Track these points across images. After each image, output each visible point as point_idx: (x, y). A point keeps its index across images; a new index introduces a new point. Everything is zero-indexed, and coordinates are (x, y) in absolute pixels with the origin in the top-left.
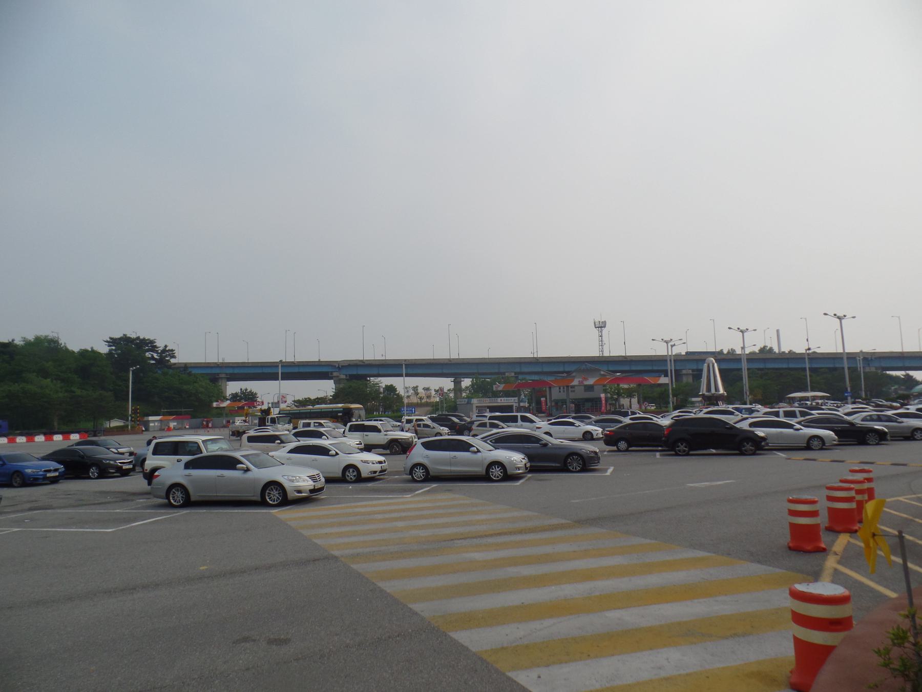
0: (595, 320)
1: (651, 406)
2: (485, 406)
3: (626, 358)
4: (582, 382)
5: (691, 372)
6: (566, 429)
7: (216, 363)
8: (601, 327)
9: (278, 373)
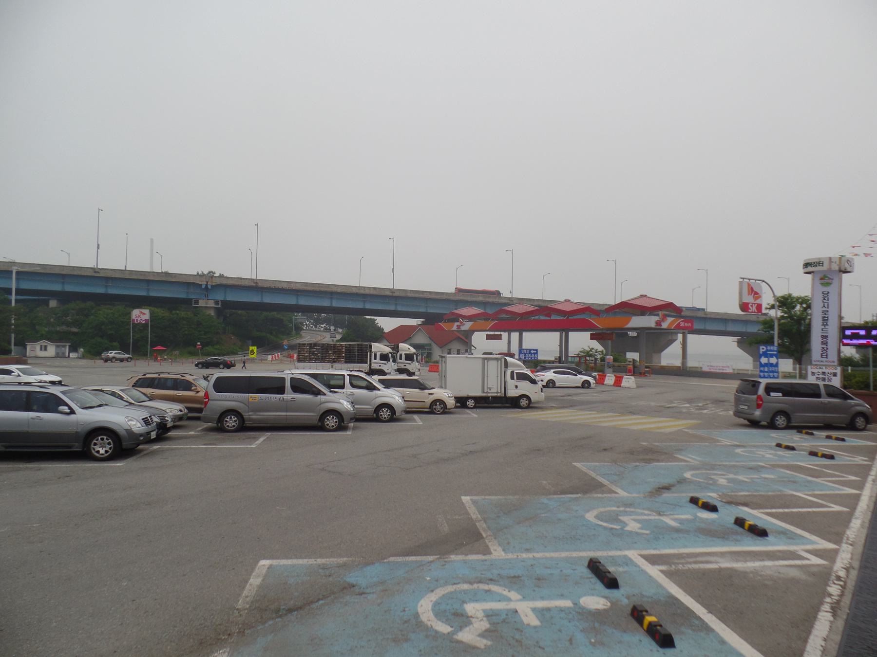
5: (213, 305)
6: (568, 377)
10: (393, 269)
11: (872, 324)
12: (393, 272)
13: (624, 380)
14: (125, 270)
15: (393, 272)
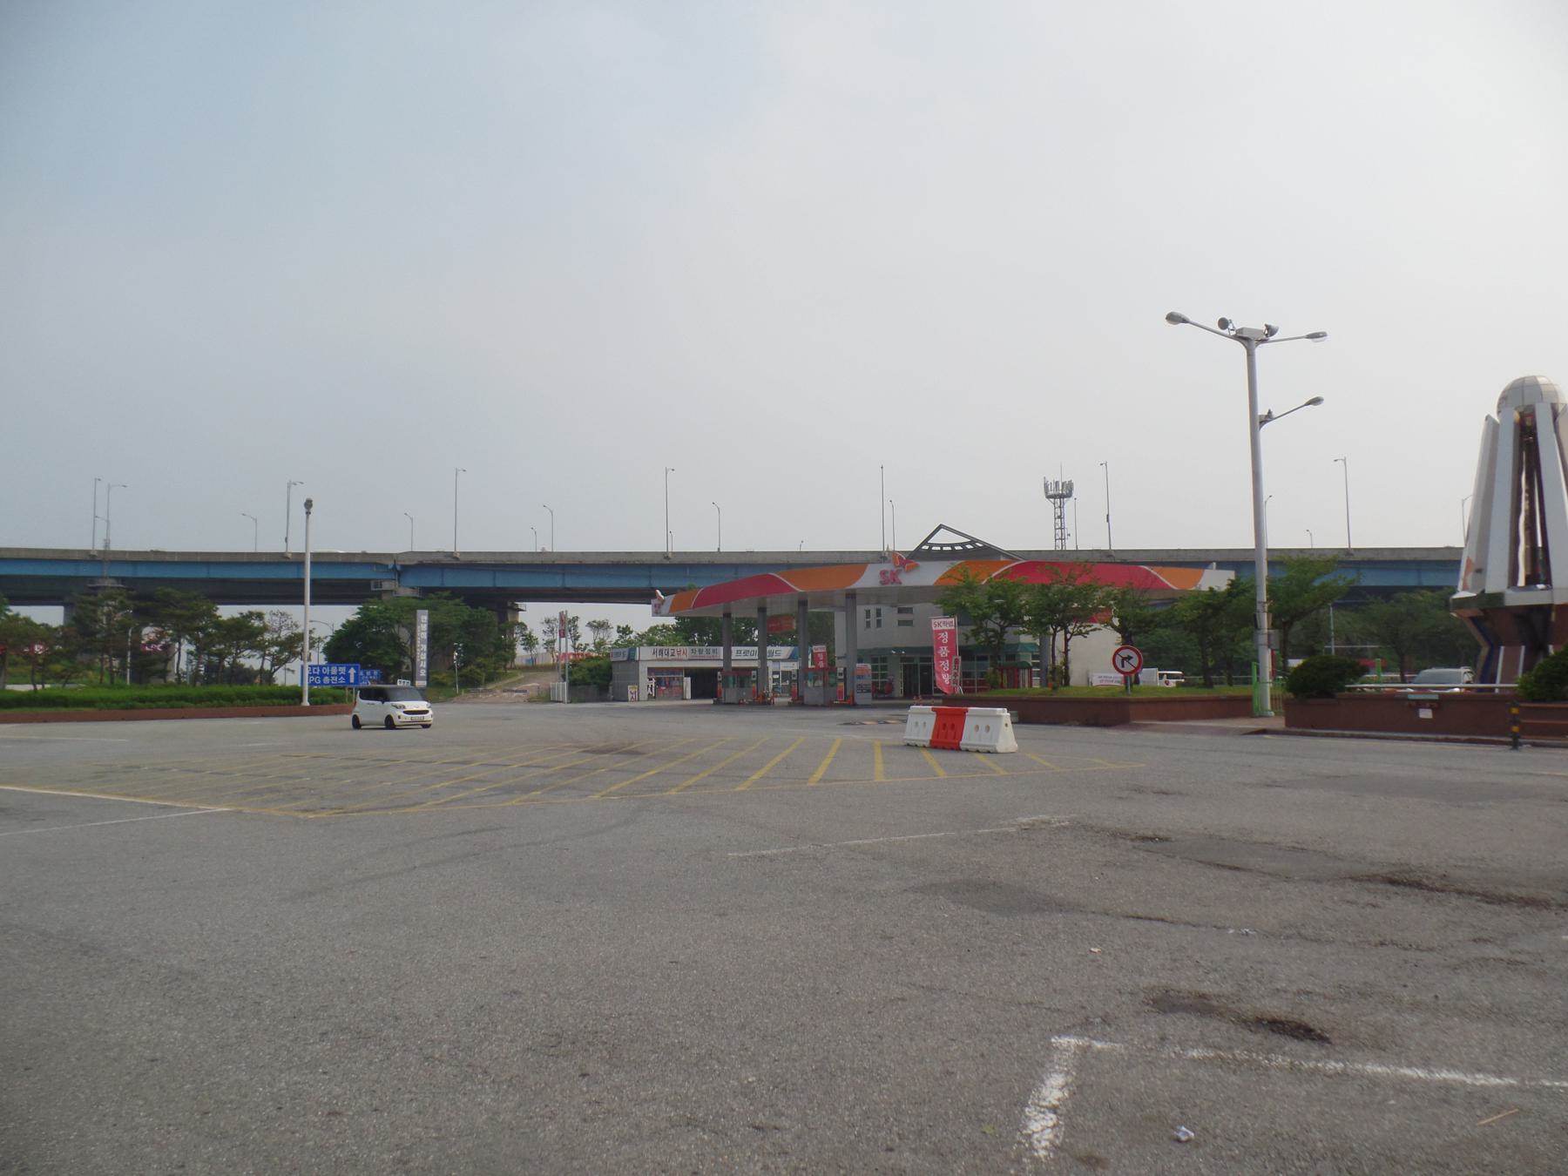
0: (1047, 479)
1: (1169, 676)
2: (680, 669)
3: (1110, 556)
4: (894, 575)
7: (87, 552)
8: (1061, 497)
9: (301, 582)
10: (1108, 516)
11: (1320, 556)
12: (1108, 521)
13: (969, 724)
14: (1077, 551)
15: (1108, 521)
